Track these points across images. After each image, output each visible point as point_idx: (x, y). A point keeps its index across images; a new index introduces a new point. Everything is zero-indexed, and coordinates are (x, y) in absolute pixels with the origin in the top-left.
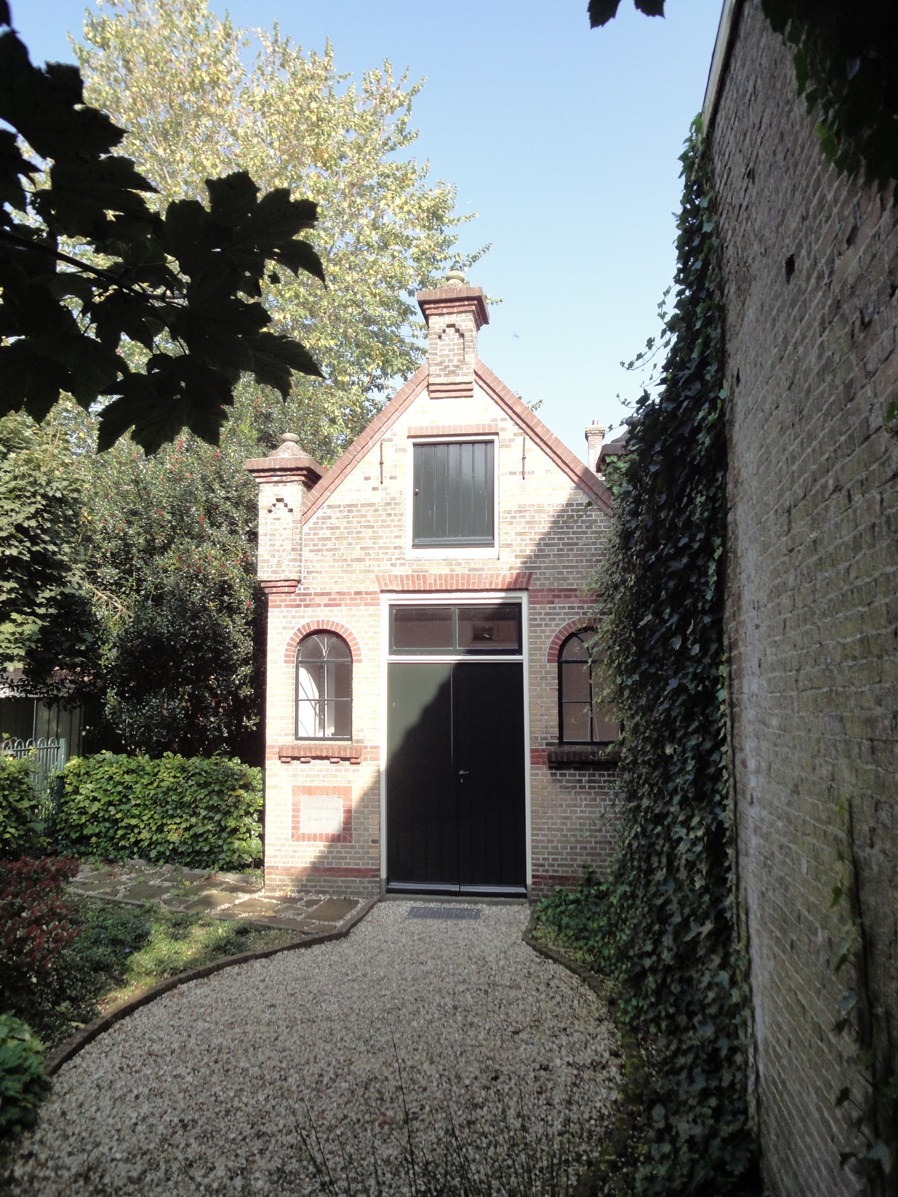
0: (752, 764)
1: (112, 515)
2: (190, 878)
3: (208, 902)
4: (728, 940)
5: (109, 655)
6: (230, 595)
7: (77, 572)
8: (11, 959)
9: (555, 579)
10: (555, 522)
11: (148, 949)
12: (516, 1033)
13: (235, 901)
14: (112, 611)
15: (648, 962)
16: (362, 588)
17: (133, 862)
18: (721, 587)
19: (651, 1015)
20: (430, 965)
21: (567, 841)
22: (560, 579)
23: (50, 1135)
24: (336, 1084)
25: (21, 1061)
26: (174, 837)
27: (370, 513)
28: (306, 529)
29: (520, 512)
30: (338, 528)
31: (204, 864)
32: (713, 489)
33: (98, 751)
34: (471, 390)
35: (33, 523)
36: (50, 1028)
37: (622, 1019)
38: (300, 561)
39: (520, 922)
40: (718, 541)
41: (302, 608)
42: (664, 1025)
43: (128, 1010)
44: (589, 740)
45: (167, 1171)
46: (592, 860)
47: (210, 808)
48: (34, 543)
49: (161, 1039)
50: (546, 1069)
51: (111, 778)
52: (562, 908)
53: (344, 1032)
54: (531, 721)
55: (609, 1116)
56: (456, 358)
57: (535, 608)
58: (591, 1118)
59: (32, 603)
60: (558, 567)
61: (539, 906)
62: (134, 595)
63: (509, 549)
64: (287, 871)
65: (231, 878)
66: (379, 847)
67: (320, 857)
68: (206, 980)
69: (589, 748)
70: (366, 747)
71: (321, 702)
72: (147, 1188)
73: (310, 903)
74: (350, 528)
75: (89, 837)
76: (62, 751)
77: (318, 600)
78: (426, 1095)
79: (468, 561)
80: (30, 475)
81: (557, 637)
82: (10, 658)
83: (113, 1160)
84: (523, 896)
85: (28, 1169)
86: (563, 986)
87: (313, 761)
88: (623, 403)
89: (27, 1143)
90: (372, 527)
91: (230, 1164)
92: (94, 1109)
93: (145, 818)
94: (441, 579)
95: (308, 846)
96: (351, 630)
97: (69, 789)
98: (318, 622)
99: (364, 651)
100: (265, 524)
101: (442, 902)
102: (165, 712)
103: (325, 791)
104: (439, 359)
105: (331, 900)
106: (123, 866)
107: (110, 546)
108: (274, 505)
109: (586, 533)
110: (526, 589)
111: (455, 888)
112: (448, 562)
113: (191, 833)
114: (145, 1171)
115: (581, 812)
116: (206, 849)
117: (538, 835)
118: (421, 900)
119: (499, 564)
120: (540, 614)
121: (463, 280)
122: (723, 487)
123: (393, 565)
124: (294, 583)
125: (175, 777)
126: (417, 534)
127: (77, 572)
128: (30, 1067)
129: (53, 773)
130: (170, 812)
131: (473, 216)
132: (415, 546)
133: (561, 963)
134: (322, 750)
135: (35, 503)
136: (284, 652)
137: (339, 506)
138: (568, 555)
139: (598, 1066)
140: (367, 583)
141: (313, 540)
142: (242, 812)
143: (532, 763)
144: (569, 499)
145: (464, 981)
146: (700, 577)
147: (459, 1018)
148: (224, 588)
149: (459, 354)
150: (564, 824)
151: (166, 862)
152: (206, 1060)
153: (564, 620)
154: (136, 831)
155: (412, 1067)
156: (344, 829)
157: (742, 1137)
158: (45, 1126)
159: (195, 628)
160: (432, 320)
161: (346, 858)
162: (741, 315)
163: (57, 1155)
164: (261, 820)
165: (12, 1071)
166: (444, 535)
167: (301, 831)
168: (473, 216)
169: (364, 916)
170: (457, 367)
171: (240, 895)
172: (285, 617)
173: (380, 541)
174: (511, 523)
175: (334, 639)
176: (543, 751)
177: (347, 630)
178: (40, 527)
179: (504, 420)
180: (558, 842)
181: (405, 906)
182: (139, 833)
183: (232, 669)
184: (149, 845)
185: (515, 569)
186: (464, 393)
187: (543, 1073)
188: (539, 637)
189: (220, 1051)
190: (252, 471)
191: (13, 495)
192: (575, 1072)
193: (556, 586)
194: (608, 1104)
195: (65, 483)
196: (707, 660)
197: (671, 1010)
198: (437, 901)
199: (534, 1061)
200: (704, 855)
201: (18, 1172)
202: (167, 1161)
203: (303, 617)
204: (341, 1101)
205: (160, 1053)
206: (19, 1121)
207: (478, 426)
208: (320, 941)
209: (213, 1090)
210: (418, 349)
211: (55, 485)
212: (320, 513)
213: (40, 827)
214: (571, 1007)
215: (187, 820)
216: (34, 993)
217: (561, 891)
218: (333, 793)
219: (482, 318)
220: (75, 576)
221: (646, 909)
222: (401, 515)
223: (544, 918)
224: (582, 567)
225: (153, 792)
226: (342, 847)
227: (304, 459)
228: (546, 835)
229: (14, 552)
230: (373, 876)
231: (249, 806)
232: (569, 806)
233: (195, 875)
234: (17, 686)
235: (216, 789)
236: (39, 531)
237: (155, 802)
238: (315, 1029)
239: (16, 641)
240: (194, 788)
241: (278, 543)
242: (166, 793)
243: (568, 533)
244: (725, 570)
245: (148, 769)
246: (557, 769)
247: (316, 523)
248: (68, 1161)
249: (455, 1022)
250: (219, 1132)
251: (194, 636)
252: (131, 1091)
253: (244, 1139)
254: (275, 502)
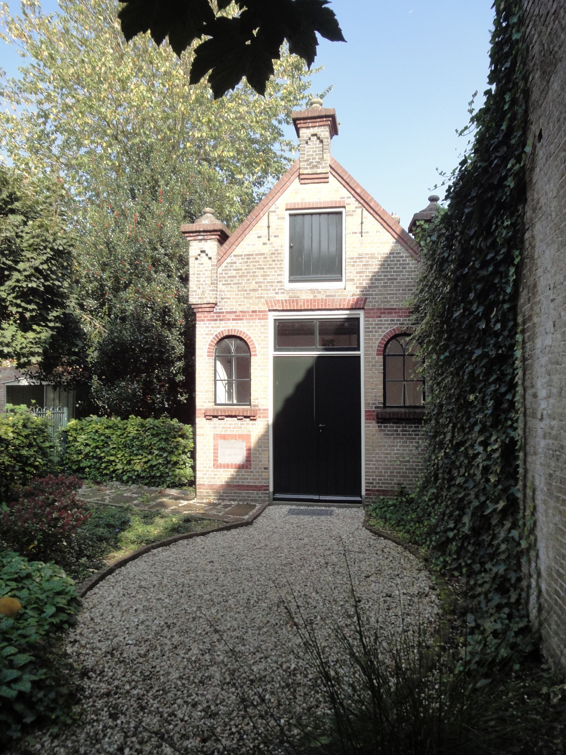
0: (542, 393)
1: (93, 265)
2: (149, 491)
3: (163, 505)
4: (517, 511)
5: (93, 355)
6: (169, 316)
7: (73, 300)
8: (51, 530)
9: (382, 302)
10: (382, 265)
11: (130, 530)
12: (368, 577)
13: (178, 505)
14: (94, 328)
15: (451, 534)
16: (256, 308)
17: (112, 483)
18: (517, 284)
19: (454, 565)
20: (306, 540)
21: (388, 468)
22: (384, 302)
23: (85, 630)
24: (259, 604)
25: (64, 588)
26: (138, 468)
27: (261, 259)
28: (220, 270)
29: (360, 258)
30: (241, 269)
31: (157, 484)
32: (515, 218)
33: (88, 415)
34: (327, 178)
35: (45, 267)
36: (76, 572)
37: (434, 569)
38: (217, 291)
39: (358, 517)
40: (517, 253)
41: (218, 322)
42: (464, 570)
43: (123, 563)
44: (402, 405)
45: (161, 651)
46: (404, 480)
47: (161, 449)
48: (46, 280)
49: (145, 579)
50: (390, 596)
51: (97, 431)
52: (385, 509)
53: (259, 576)
54: (365, 392)
55: (435, 621)
56: (317, 157)
57: (369, 321)
58: (423, 623)
59: (46, 320)
60: (384, 294)
61: (370, 508)
62: (107, 318)
63: (352, 283)
64: (211, 487)
65: (174, 492)
66: (268, 472)
67: (231, 478)
68: (168, 547)
69: (403, 410)
70: (260, 410)
71: (230, 384)
72: (151, 660)
73: (226, 506)
74: (249, 269)
75: (84, 468)
76: (65, 415)
77: (228, 316)
78: (316, 610)
79: (325, 291)
80: (43, 235)
81: (382, 339)
82: (33, 354)
83: (127, 644)
84: (360, 502)
85: (75, 649)
86: (393, 552)
87: (226, 419)
88: (440, 174)
89: (72, 635)
90: (263, 269)
91: (201, 647)
92: (110, 617)
93: (119, 456)
94: (307, 302)
95: (224, 472)
96: (249, 335)
97: (71, 438)
98: (228, 330)
99: (258, 348)
100: (194, 268)
101: (309, 506)
102: (129, 390)
103: (233, 437)
104: (306, 158)
105: (238, 505)
106: (106, 486)
107: (90, 287)
108: (199, 255)
109: (402, 272)
110: (363, 309)
111: (316, 497)
112: (312, 291)
113: (149, 464)
114: (148, 651)
115: (397, 450)
116: (158, 474)
117: (369, 464)
118: (295, 505)
119: (345, 293)
120: (372, 324)
121: (321, 105)
122: (522, 216)
123: (276, 293)
124: (213, 305)
125: (137, 430)
126: (292, 273)
127: (73, 300)
128: (69, 591)
129: (61, 429)
130: (135, 452)
131: (321, 68)
132: (291, 281)
133: (389, 539)
134: (232, 411)
135: (46, 253)
136: (207, 350)
137: (242, 255)
138: (390, 286)
139: (422, 595)
140: (260, 305)
141: (224, 277)
142: (181, 452)
143: (366, 419)
144: (392, 250)
145: (329, 549)
146: (501, 278)
147: (330, 569)
148: (166, 311)
149: (320, 154)
150: (387, 457)
151: (133, 483)
152: (175, 590)
153: (388, 328)
154: (114, 464)
155: (305, 595)
156: (247, 461)
157: (525, 631)
158: (82, 625)
159: (146, 337)
160: (302, 131)
161: (247, 479)
162: (545, 92)
163: (92, 641)
164: (193, 456)
165: (59, 593)
166: (309, 274)
167: (219, 462)
168: (321, 68)
169: (260, 513)
170: (318, 162)
171: (182, 501)
172: (207, 327)
173: (268, 278)
174: (353, 266)
175: (239, 341)
176: (373, 411)
177: (247, 335)
178: (50, 269)
179: (348, 198)
180: (382, 468)
181: (285, 508)
182: (116, 465)
183: (173, 363)
184: (122, 473)
185: (356, 295)
186: (323, 180)
187: (388, 598)
188: (371, 339)
189: (183, 586)
190: (184, 233)
191: (32, 248)
192: (409, 598)
193: (382, 306)
194: (433, 615)
195: (65, 241)
196: (506, 333)
197: (469, 562)
198: (305, 505)
199: (382, 592)
200: (499, 461)
201: (69, 651)
202: (161, 645)
203: (219, 327)
204: (263, 613)
205: (146, 586)
206: (66, 622)
207: (332, 202)
208: (236, 527)
209: (183, 607)
210: (285, 158)
211: (58, 242)
212: (229, 260)
213: (56, 459)
214: (400, 563)
215: (146, 457)
216: (64, 552)
217: (383, 499)
218: (239, 438)
219: (334, 130)
220: (72, 303)
221: (449, 502)
222: (282, 260)
223: (374, 515)
224: (400, 294)
225: (123, 440)
226: (245, 472)
227: (219, 225)
228: (374, 465)
229: (34, 285)
230: (265, 490)
231: (185, 447)
232: (389, 446)
233: (152, 490)
234: (35, 377)
235: (164, 437)
236: (49, 272)
237: (125, 446)
238: (240, 575)
239: (36, 343)
240: (150, 437)
241: (202, 280)
242: (132, 440)
243: (391, 272)
244: (521, 271)
245: (120, 425)
246: (382, 423)
247: (227, 267)
248: (99, 645)
249: (328, 571)
250: (191, 629)
251: (147, 343)
252: (132, 607)
253: (207, 633)
254: (199, 253)
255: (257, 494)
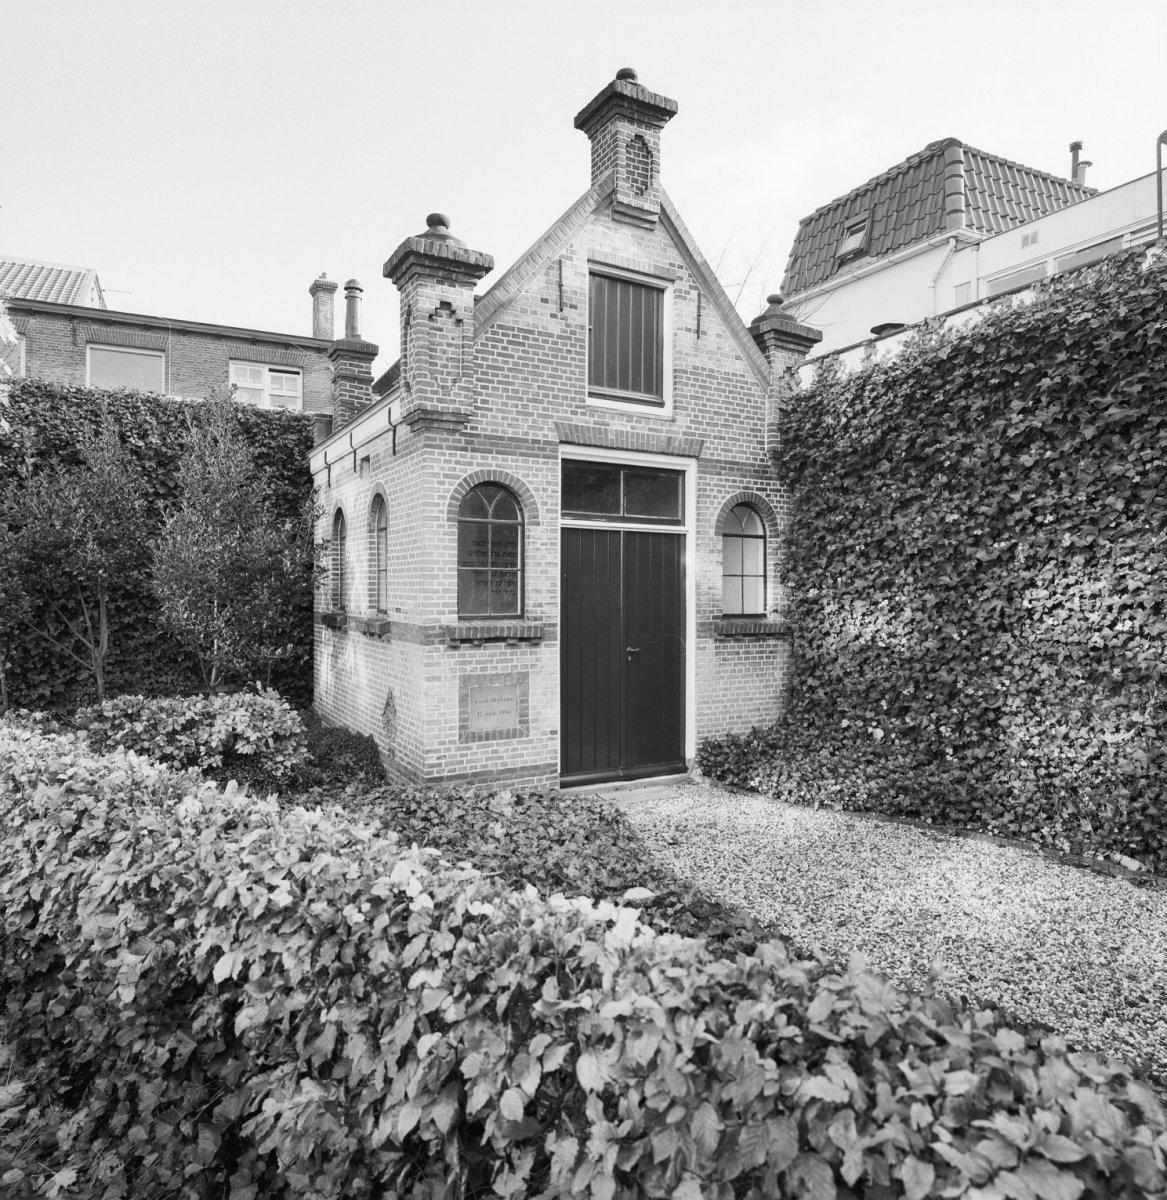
172: (446, 461)
203: (470, 464)
255: (539, 781)
